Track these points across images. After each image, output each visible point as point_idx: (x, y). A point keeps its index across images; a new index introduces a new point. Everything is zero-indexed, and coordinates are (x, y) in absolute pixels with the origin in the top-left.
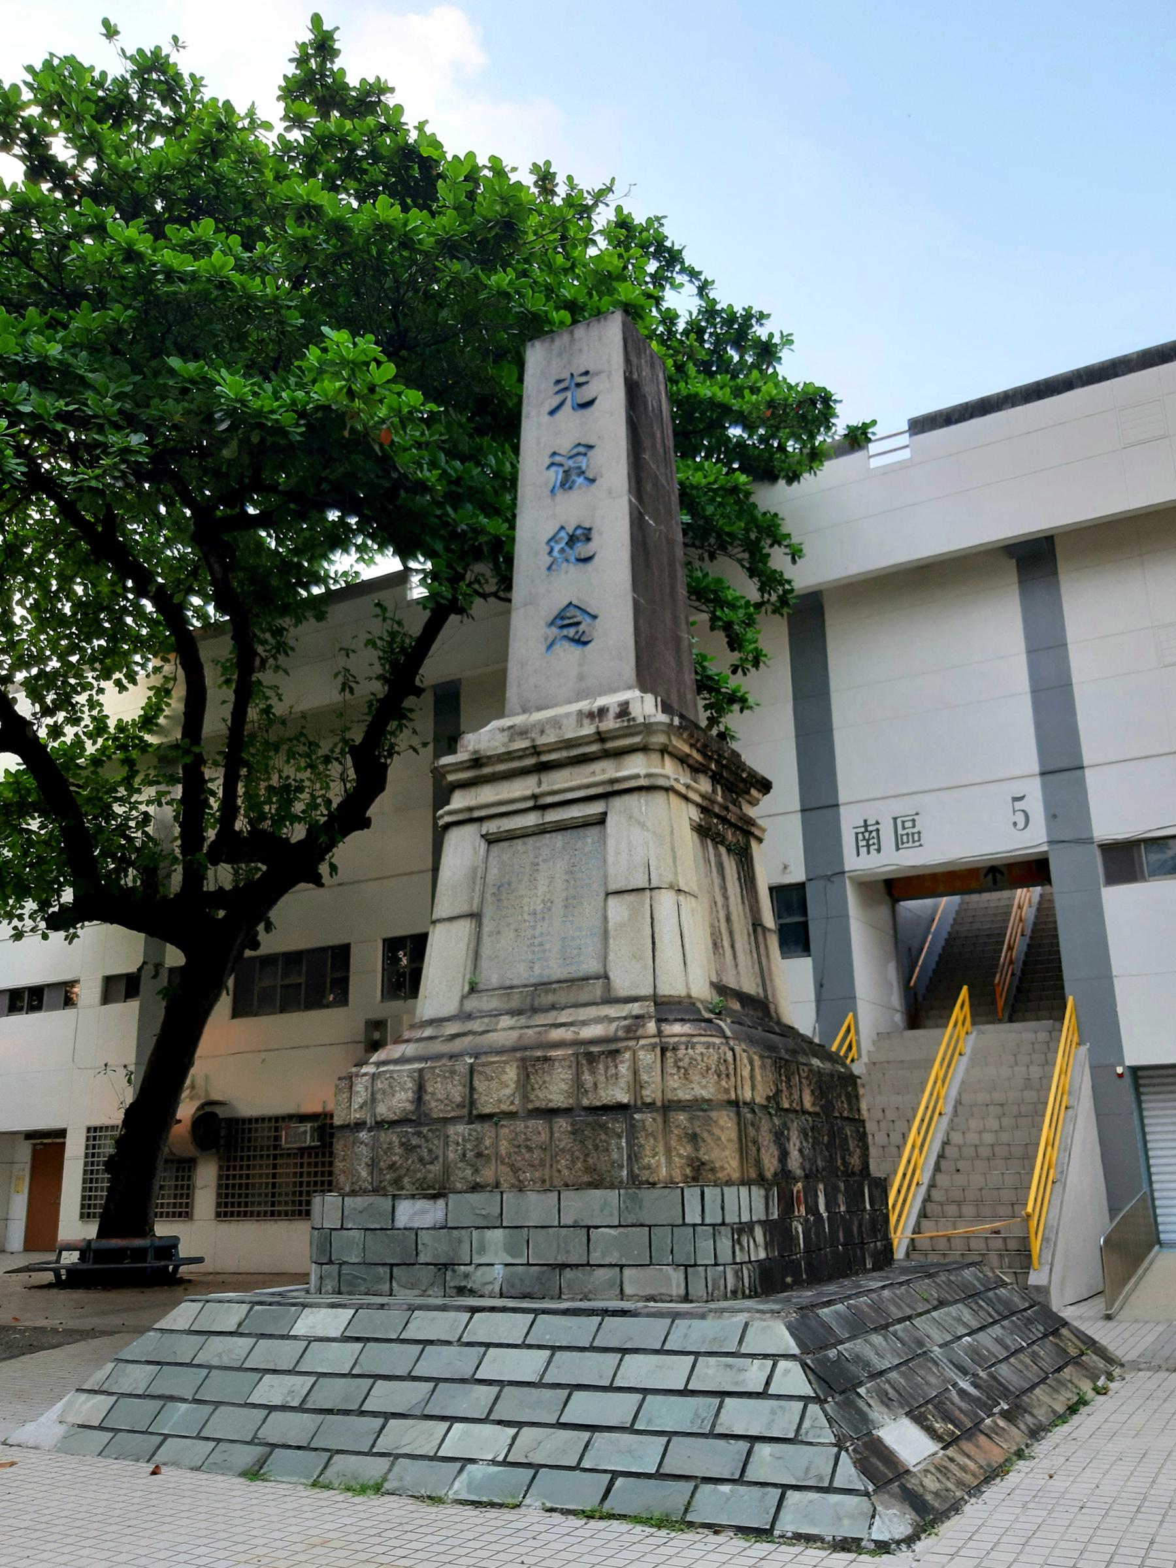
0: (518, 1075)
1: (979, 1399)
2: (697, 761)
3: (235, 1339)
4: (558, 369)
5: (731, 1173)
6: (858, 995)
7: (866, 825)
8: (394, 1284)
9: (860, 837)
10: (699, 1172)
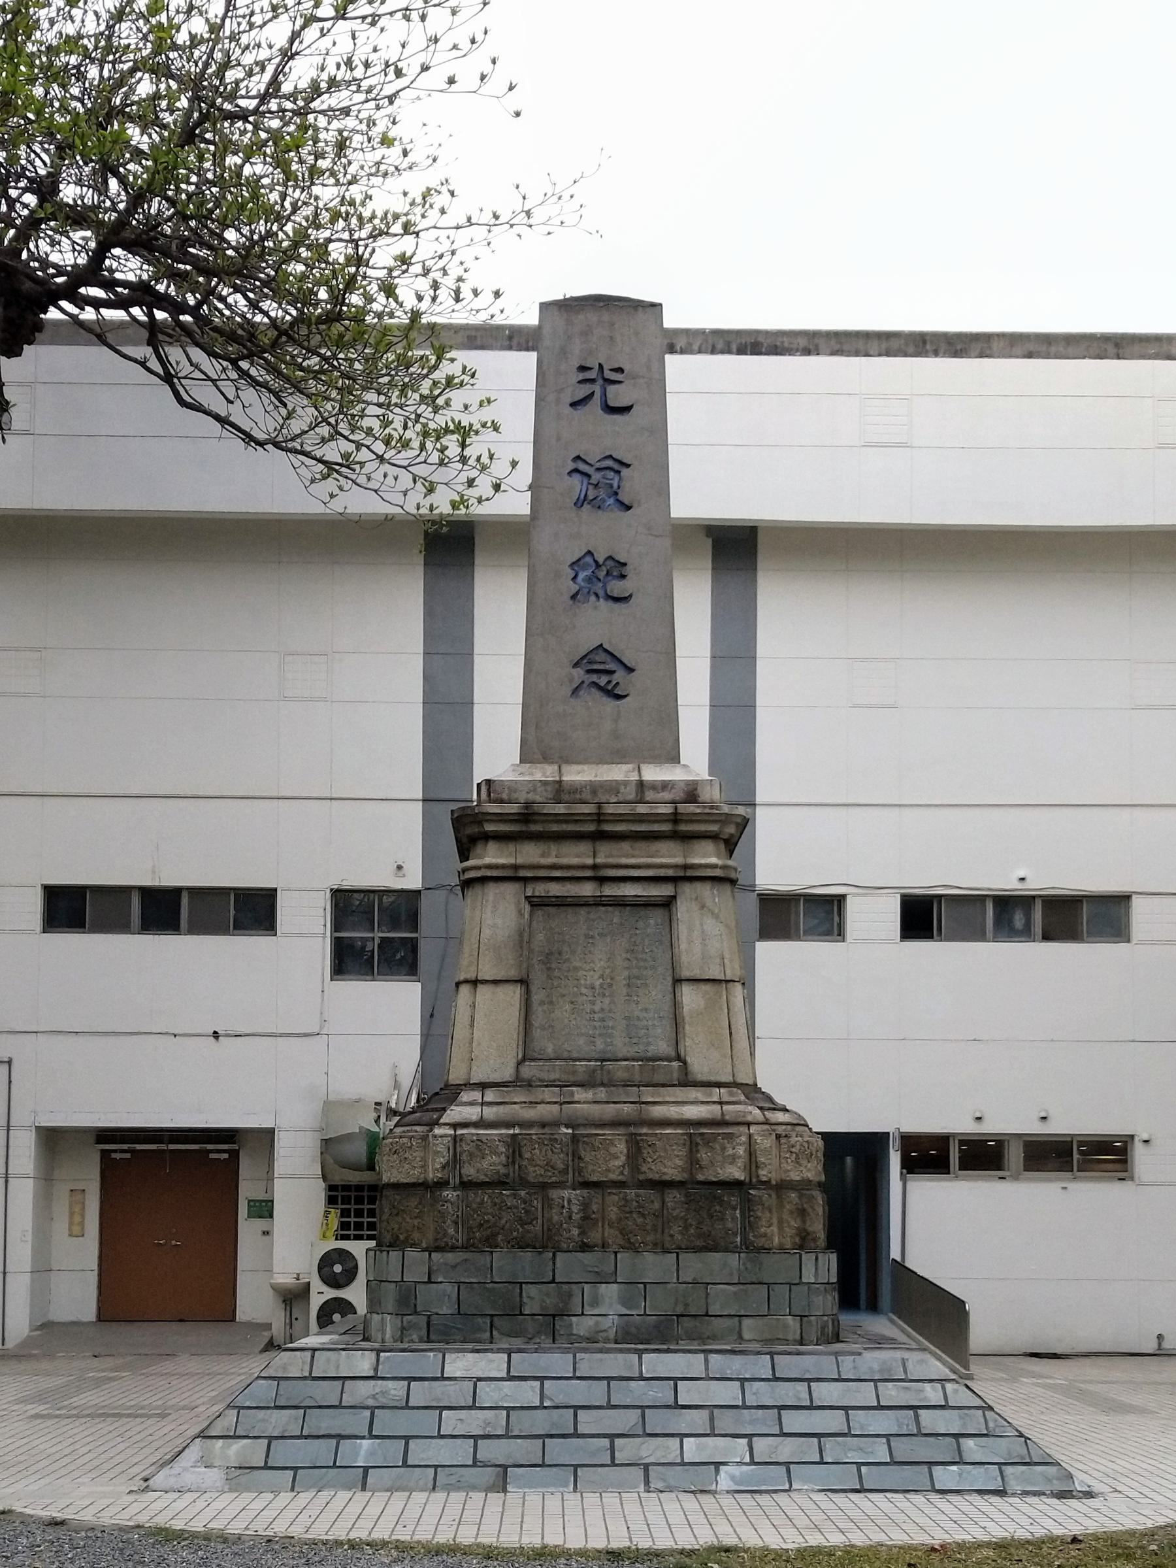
3: (373, 1382)
8: (495, 1333)
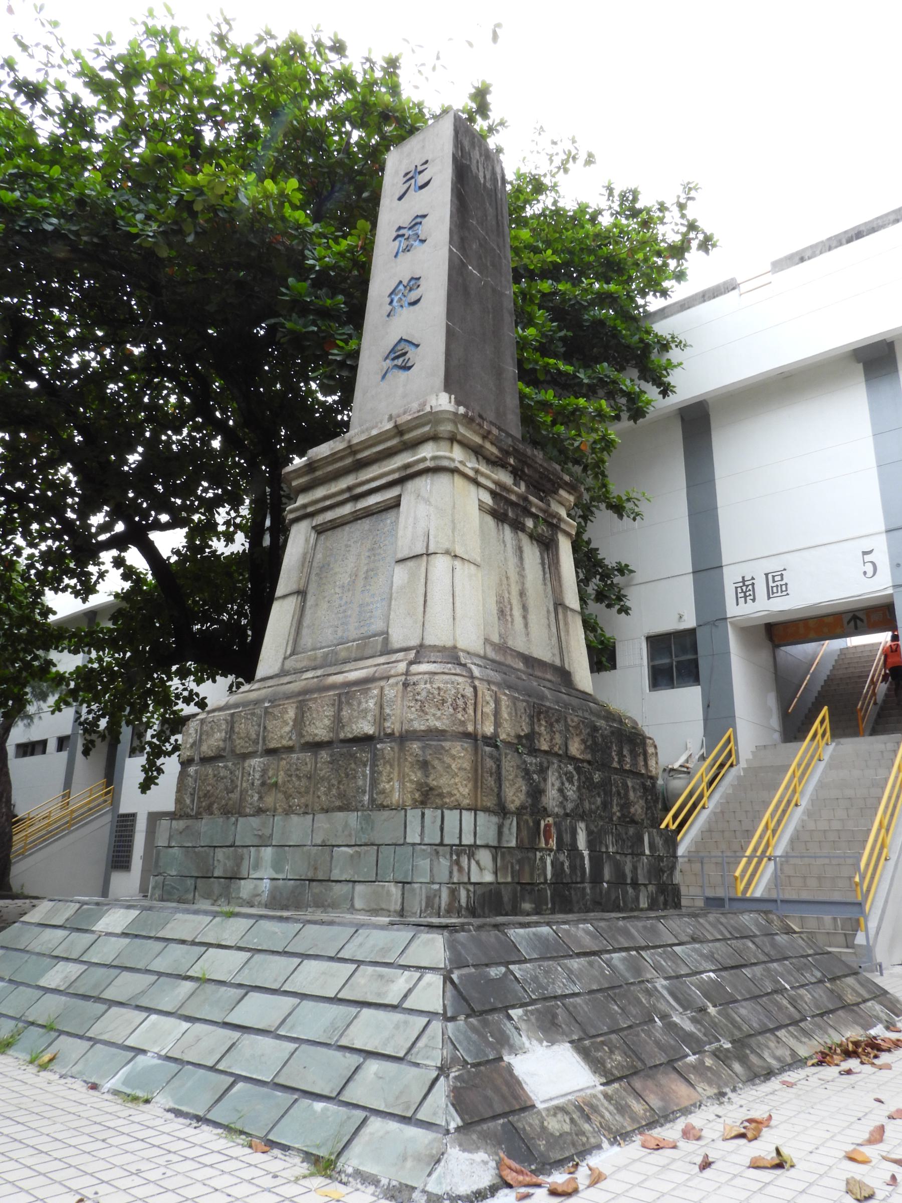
0: (296, 714)
1: (690, 1035)
2: (492, 453)
4: (407, 165)
5: (461, 799)
6: (737, 714)
7: (744, 581)
9: (739, 590)
10: (427, 796)
